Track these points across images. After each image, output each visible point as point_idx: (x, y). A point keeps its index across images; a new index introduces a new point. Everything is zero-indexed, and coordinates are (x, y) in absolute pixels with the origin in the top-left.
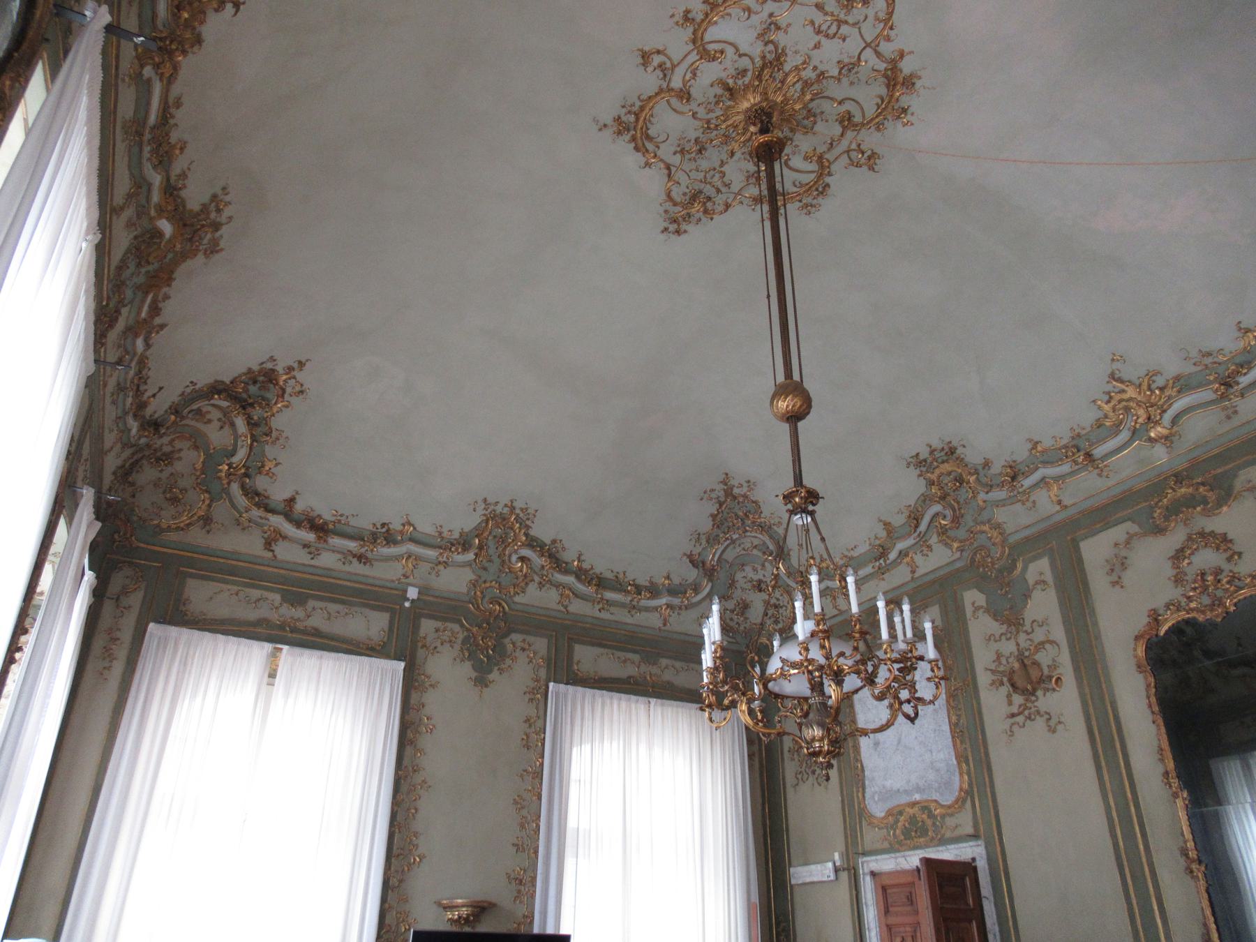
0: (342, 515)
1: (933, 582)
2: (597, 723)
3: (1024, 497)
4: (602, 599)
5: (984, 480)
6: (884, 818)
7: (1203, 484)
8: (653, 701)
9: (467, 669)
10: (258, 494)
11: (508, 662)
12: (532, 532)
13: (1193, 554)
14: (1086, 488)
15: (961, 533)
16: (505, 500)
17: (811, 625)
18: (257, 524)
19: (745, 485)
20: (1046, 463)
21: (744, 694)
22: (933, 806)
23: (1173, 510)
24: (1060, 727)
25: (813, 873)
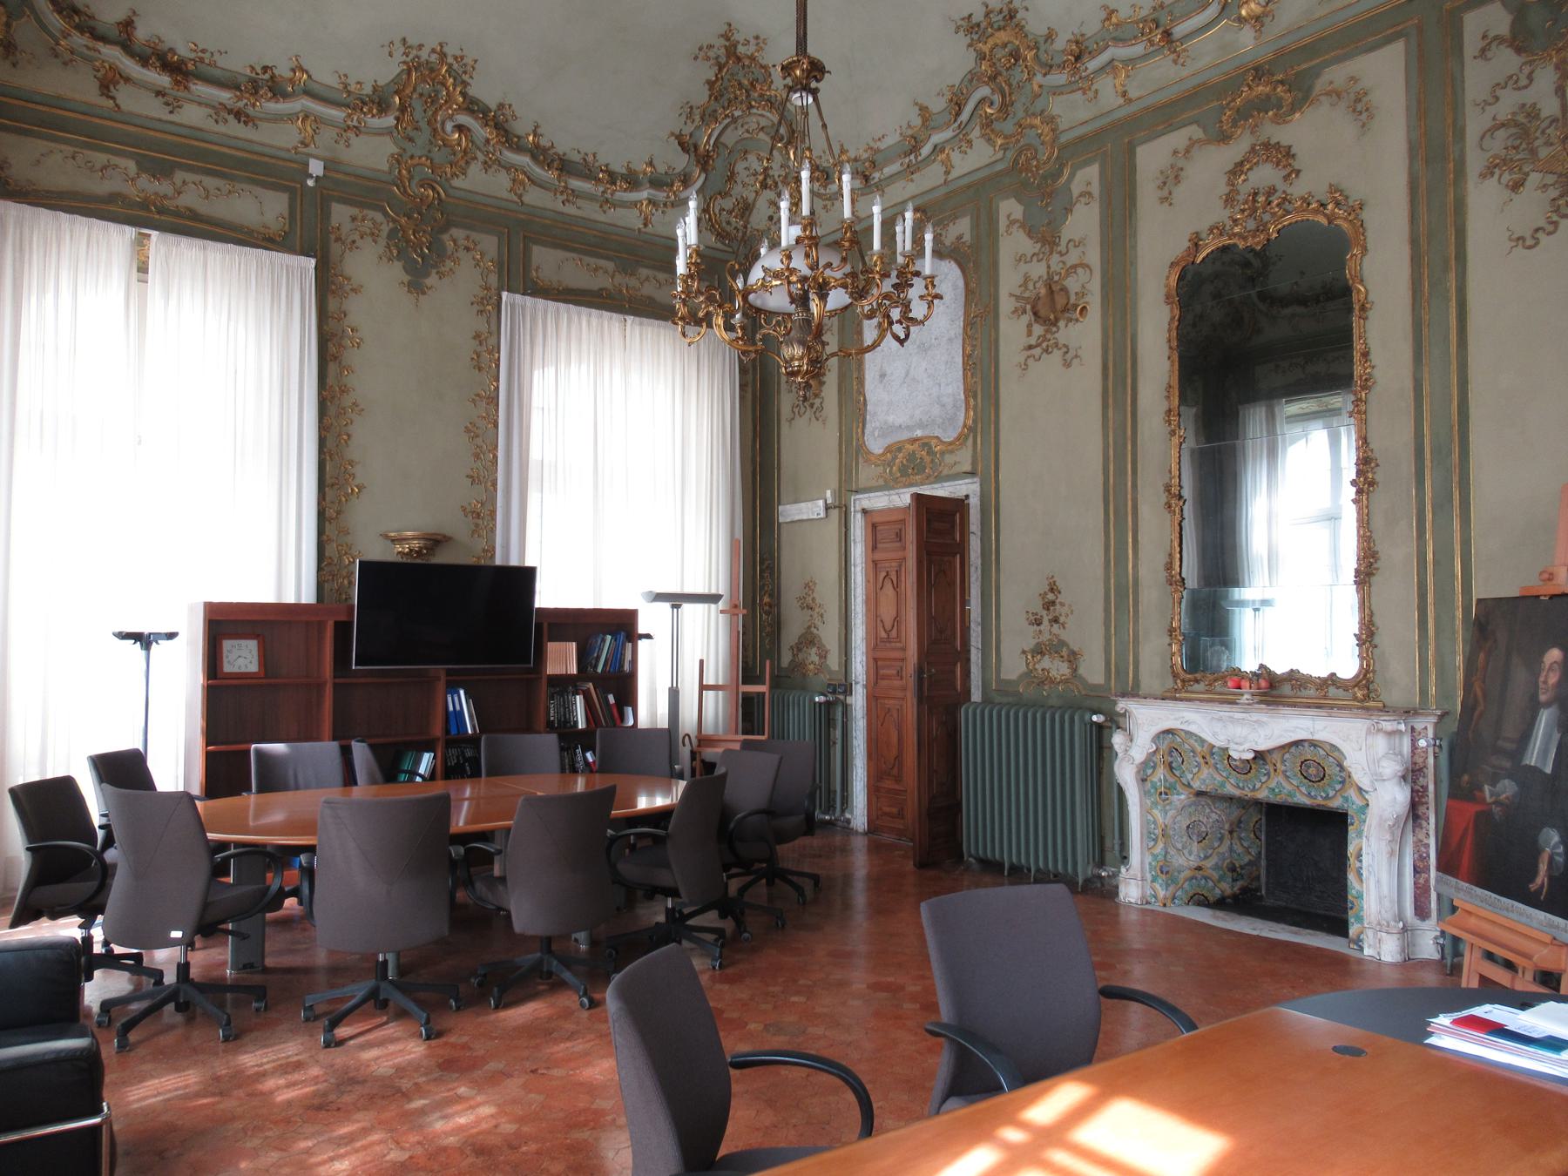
0: (203, 51)
1: (969, 186)
2: (563, 344)
3: (1082, 84)
4: (566, 187)
5: (1043, 57)
6: (883, 454)
7: (1282, 82)
8: (630, 319)
9: (396, 271)
10: (76, 11)
11: (450, 264)
12: (471, 91)
13: (1250, 169)
14: (1159, 76)
15: (1008, 127)
16: (431, 42)
17: (796, 231)
18: (86, 59)
19: (753, 42)
20: (1118, 40)
21: (720, 306)
22: (933, 443)
23: (1242, 115)
24: (1075, 361)
25: (802, 511)
